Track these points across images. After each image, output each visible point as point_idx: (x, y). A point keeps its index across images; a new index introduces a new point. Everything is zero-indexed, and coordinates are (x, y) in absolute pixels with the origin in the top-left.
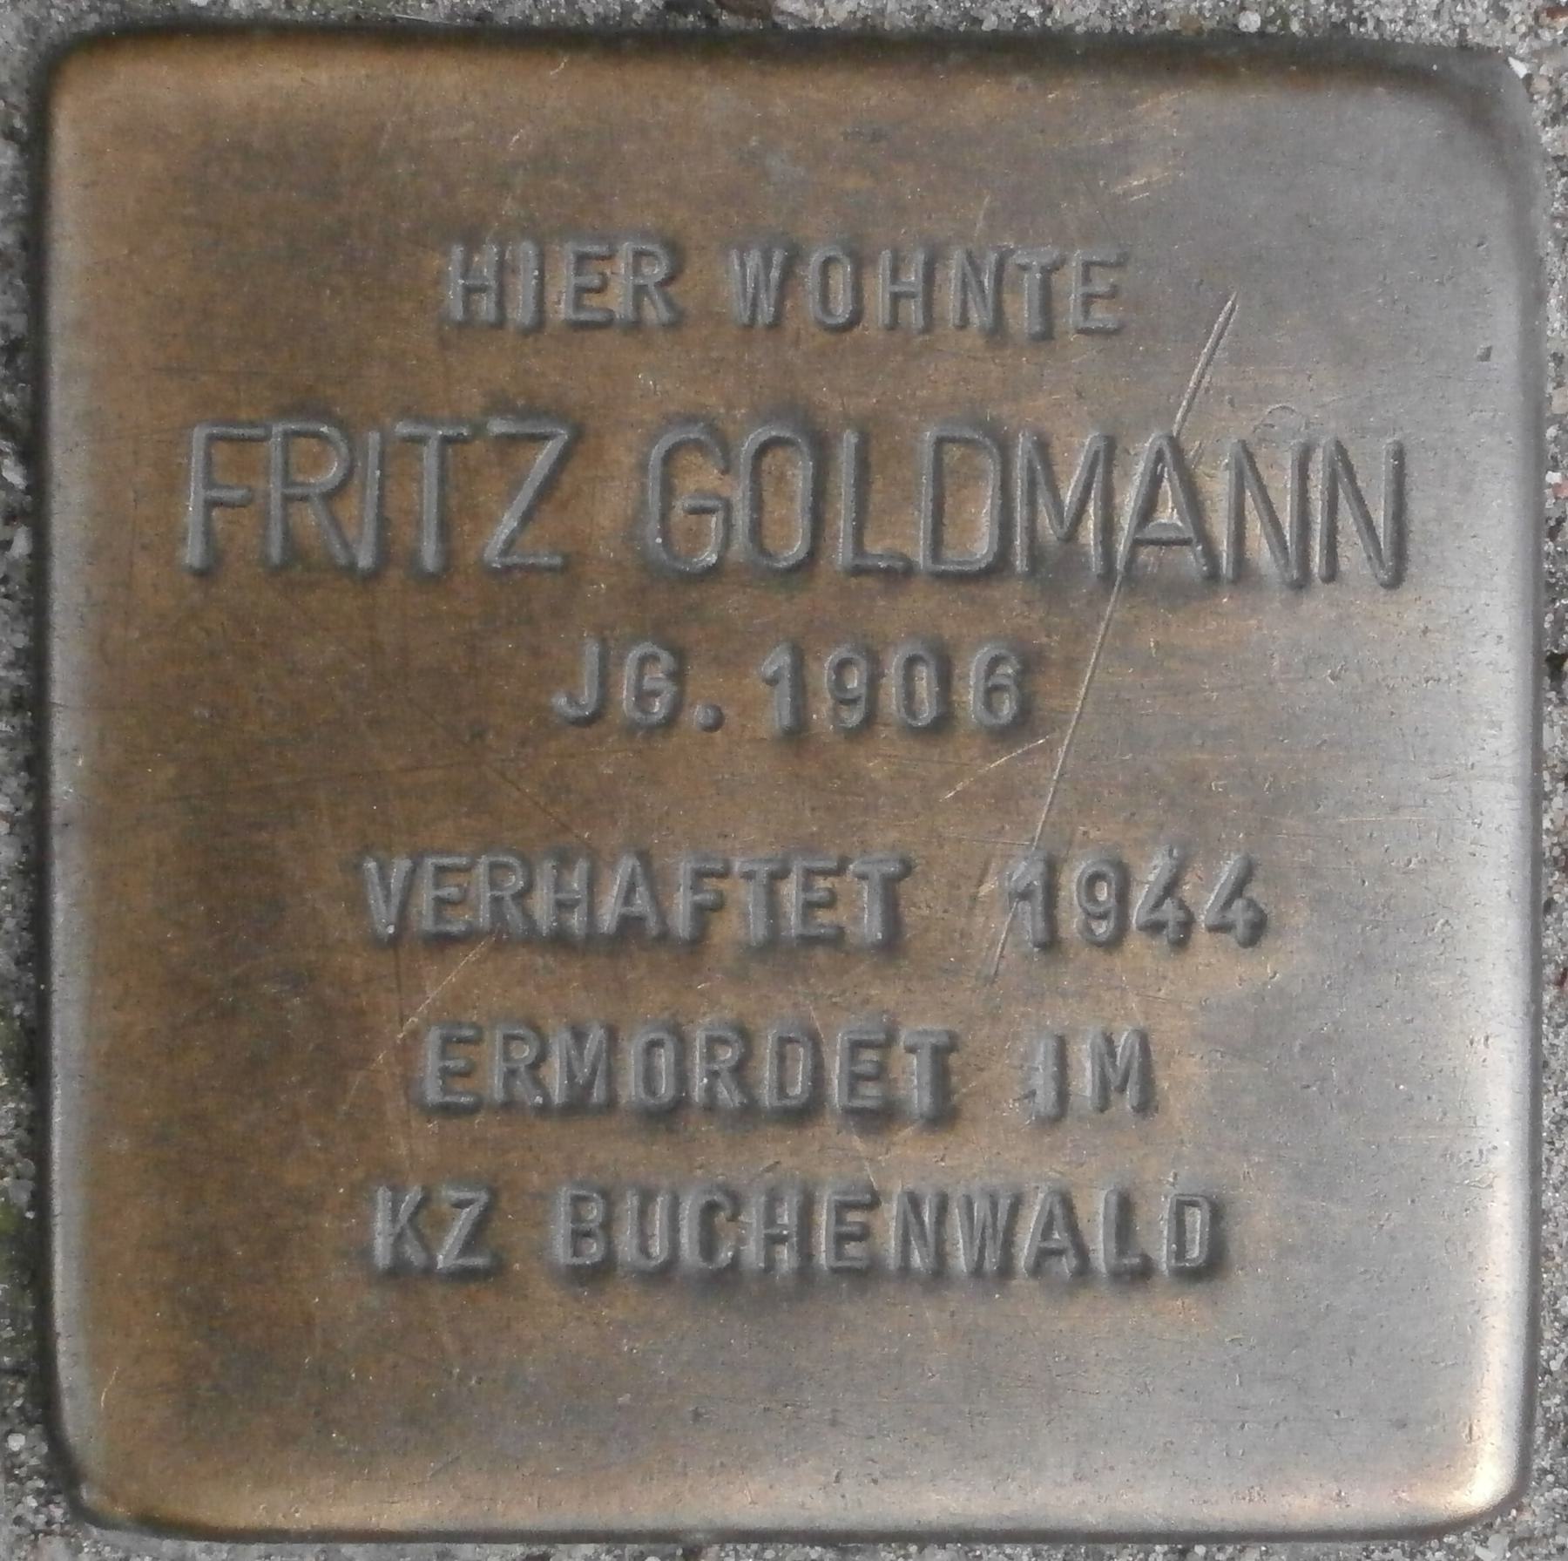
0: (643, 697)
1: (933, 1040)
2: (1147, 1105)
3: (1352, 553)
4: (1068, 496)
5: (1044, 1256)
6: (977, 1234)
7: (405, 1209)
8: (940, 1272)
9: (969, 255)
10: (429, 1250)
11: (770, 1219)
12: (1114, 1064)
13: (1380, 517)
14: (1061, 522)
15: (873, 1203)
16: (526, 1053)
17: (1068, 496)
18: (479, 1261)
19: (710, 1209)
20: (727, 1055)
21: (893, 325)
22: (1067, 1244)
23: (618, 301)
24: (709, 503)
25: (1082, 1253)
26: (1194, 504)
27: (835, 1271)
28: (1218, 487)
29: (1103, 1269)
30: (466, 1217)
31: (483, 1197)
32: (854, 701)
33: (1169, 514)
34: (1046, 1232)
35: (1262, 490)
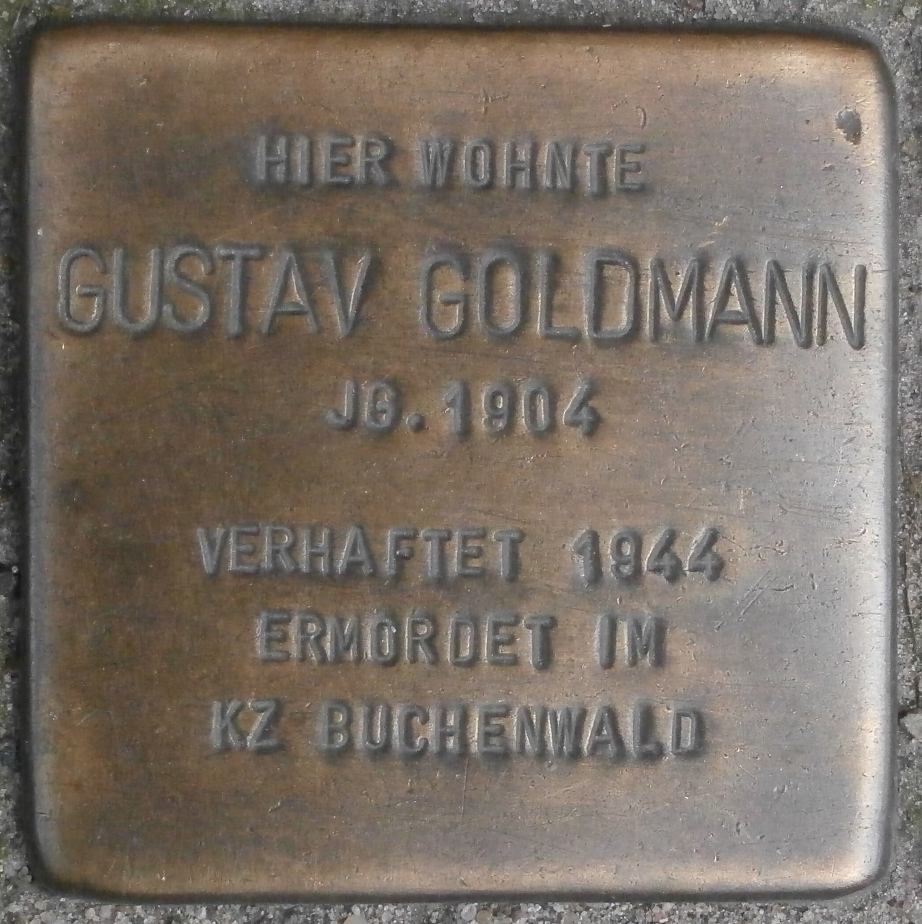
0: (375, 414)
1: (543, 623)
2: (660, 661)
3: (784, 328)
4: (678, 291)
5: (596, 746)
6: (559, 730)
7: (230, 711)
8: (542, 754)
9: (557, 146)
10: (242, 735)
11: (443, 721)
12: (640, 637)
13: (852, 312)
14: (673, 310)
15: (506, 714)
16: (313, 628)
17: (678, 291)
18: (271, 742)
19: (410, 717)
20: (424, 630)
21: (513, 186)
22: (611, 737)
23: (358, 170)
24: (94, 290)
25: (619, 741)
26: (748, 298)
27: (485, 754)
28: (760, 288)
29: (632, 751)
30: (261, 718)
31: (272, 706)
32: (500, 417)
33: (736, 305)
34: (598, 731)
35: (837, 289)
